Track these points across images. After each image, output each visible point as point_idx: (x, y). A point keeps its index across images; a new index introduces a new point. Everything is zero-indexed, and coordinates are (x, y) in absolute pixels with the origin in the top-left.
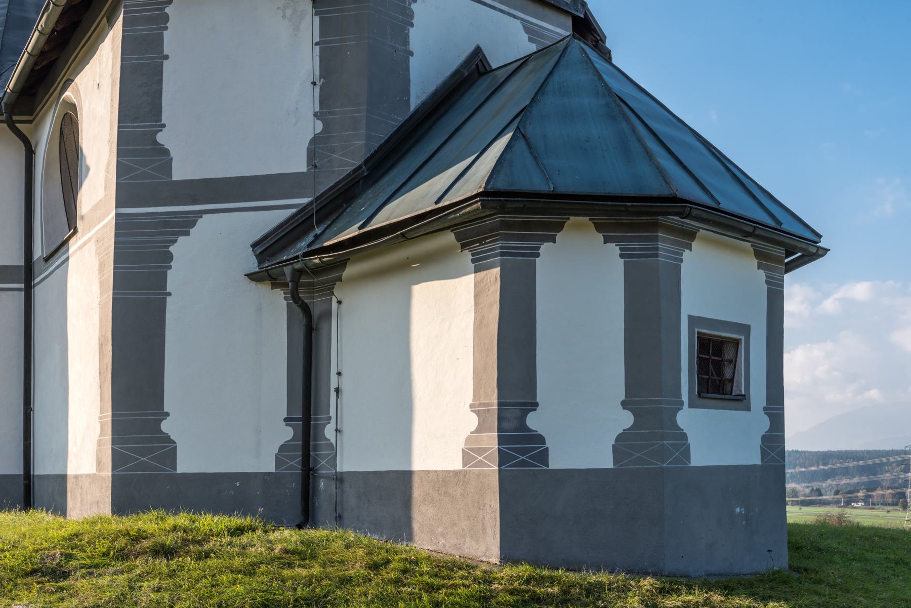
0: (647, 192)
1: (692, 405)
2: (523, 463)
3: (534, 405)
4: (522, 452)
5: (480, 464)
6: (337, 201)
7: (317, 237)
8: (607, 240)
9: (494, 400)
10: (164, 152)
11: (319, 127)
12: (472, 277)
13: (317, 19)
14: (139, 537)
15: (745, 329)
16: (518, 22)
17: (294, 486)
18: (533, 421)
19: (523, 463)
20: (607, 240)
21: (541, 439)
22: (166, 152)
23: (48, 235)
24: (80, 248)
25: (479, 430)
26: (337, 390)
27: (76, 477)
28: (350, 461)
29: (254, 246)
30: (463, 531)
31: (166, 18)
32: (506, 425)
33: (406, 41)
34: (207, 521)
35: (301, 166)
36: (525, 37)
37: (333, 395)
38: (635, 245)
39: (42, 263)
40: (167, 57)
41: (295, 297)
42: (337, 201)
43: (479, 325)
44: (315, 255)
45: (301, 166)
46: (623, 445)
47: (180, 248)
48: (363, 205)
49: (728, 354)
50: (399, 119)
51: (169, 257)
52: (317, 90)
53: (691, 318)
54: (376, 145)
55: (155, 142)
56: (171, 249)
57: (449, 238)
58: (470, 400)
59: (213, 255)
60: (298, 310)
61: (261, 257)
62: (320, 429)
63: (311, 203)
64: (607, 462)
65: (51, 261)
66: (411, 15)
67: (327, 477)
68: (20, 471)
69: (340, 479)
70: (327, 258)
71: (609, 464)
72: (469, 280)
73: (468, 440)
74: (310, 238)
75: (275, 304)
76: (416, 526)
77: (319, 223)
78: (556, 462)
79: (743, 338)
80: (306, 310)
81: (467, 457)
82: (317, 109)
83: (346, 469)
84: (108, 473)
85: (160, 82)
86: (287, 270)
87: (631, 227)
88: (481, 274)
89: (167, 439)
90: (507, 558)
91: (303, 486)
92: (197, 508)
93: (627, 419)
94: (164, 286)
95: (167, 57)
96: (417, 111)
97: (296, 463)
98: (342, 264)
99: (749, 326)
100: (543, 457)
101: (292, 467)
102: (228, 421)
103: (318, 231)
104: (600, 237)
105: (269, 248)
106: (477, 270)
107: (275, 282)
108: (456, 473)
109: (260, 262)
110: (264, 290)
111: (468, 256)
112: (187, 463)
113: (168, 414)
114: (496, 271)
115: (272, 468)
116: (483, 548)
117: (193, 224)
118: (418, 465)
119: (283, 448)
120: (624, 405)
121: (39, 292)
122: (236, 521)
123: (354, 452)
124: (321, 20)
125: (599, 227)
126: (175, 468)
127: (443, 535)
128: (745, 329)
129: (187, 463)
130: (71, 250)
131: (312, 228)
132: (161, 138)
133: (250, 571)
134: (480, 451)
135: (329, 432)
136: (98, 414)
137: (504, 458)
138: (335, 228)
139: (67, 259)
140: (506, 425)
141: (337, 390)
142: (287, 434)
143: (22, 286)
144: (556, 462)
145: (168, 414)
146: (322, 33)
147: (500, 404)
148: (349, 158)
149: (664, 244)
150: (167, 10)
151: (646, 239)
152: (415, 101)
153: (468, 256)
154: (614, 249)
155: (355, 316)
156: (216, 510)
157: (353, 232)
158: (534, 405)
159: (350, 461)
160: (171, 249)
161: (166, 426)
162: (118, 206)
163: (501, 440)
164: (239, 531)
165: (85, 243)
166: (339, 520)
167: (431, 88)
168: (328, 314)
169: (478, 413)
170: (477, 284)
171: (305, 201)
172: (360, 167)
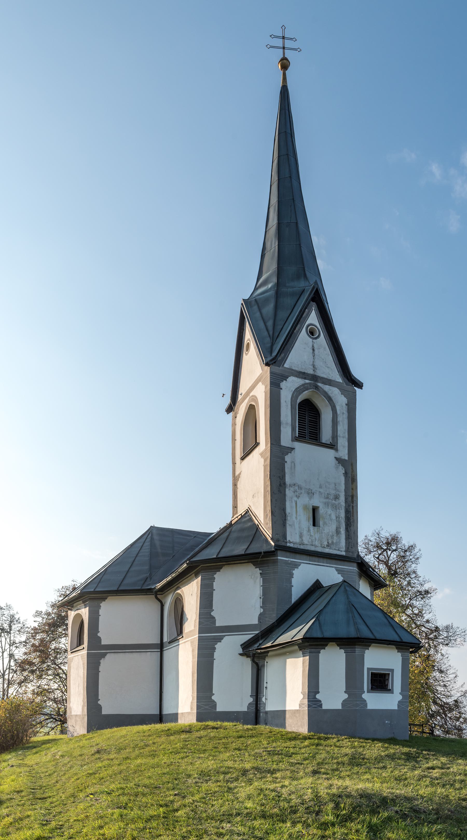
0: (351, 637)
1: (368, 692)
2: (315, 707)
3: (318, 692)
4: (315, 704)
5: (303, 707)
6: (268, 632)
7: (260, 644)
8: (340, 648)
9: (307, 691)
10: (214, 618)
11: (262, 610)
12: (302, 658)
13: (261, 579)
14: (208, 726)
15: (392, 671)
16: (334, 569)
17: (253, 715)
18: (318, 696)
19: (315, 707)
20: (340, 648)
21: (320, 701)
22: (214, 618)
23: (169, 634)
24: (185, 642)
25: (303, 699)
26: (266, 687)
27: (182, 713)
28: (269, 708)
29: (241, 645)
30: (298, 724)
31: (214, 578)
32: (310, 697)
33: (291, 583)
34: (226, 724)
35: (256, 622)
36: (336, 572)
37: (265, 688)
38: (349, 650)
39: (167, 643)
40: (214, 590)
41: (253, 661)
42: (268, 632)
43: (303, 671)
44: (257, 651)
45: (256, 622)
46: (344, 703)
47: (218, 646)
48: (274, 635)
49: (387, 678)
50: (288, 607)
51: (215, 648)
52: (261, 600)
53: (368, 669)
54: (280, 616)
55: (211, 615)
56: (215, 646)
57: (297, 647)
58: (301, 691)
59: (228, 650)
60: (255, 665)
61: (243, 649)
62: (261, 699)
63: (259, 633)
64: (340, 707)
65: (171, 644)
66: (293, 574)
67: (263, 712)
68: (158, 713)
69: (266, 713)
70: (262, 651)
71: (340, 708)
72: (301, 659)
73: (300, 701)
74: (258, 644)
75: (248, 662)
76: (287, 725)
77: (261, 639)
78: (324, 707)
79: (391, 673)
80: (257, 664)
81: (300, 706)
82: (261, 605)
83: (268, 710)
84: (195, 711)
85: (212, 597)
86: (251, 654)
87: (348, 645)
88: (304, 658)
89: (214, 701)
90: (309, 731)
91: (256, 714)
92: (223, 721)
93: (346, 696)
94: (213, 657)
95: (214, 590)
96: (294, 603)
97: (253, 708)
98: (268, 652)
99: (393, 670)
100: (366, 705)
101: (252, 710)
102: (232, 694)
103: (261, 642)
104: (339, 648)
105: (246, 646)
106: (303, 657)
107: (248, 656)
108: (297, 710)
109: (243, 650)
110: (244, 659)
111: (301, 652)
112: (219, 709)
113: (214, 694)
114: (308, 657)
115: (246, 710)
116: (304, 730)
117: (222, 639)
118: (288, 708)
119: (249, 704)
120: (345, 692)
121: (166, 653)
122: (234, 724)
123: (270, 704)
124: (263, 579)
125: (338, 645)
126: (216, 709)
127: (294, 727)
128: (392, 671)
129: (219, 709)
130: (180, 643)
131: (258, 641)
132: (212, 614)
133: (238, 732)
134: (303, 704)
135: (264, 699)
136: (191, 694)
137: (309, 706)
138: (265, 642)
139: (179, 645)
140: (310, 697)
141: (266, 687)
142: (251, 700)
143: (159, 650)
144: (324, 707)
145: (214, 694)
146: (263, 582)
147: (308, 692)
148: (272, 619)
149: (358, 650)
150: (215, 576)
151: (352, 648)
152: (293, 601)
153: (301, 652)
154: (343, 651)
155: (271, 668)
156: (228, 721)
157: (269, 644)
158: (318, 692)
159: (269, 708)
160: (215, 646)
161: (213, 698)
162: (199, 633)
163: (309, 701)
164: (235, 725)
165: (186, 642)
166: (266, 724)
167: (300, 595)
168: (263, 666)
169: (303, 694)
170: (303, 660)
171: (257, 632)
172: (274, 623)
